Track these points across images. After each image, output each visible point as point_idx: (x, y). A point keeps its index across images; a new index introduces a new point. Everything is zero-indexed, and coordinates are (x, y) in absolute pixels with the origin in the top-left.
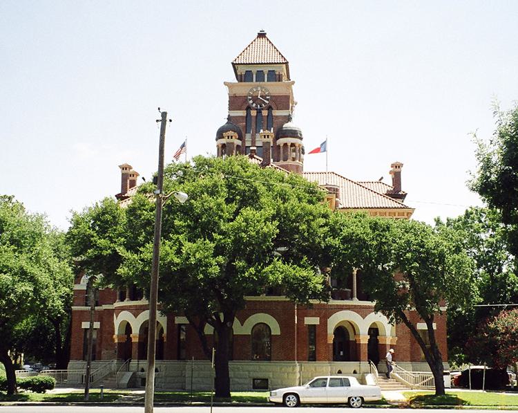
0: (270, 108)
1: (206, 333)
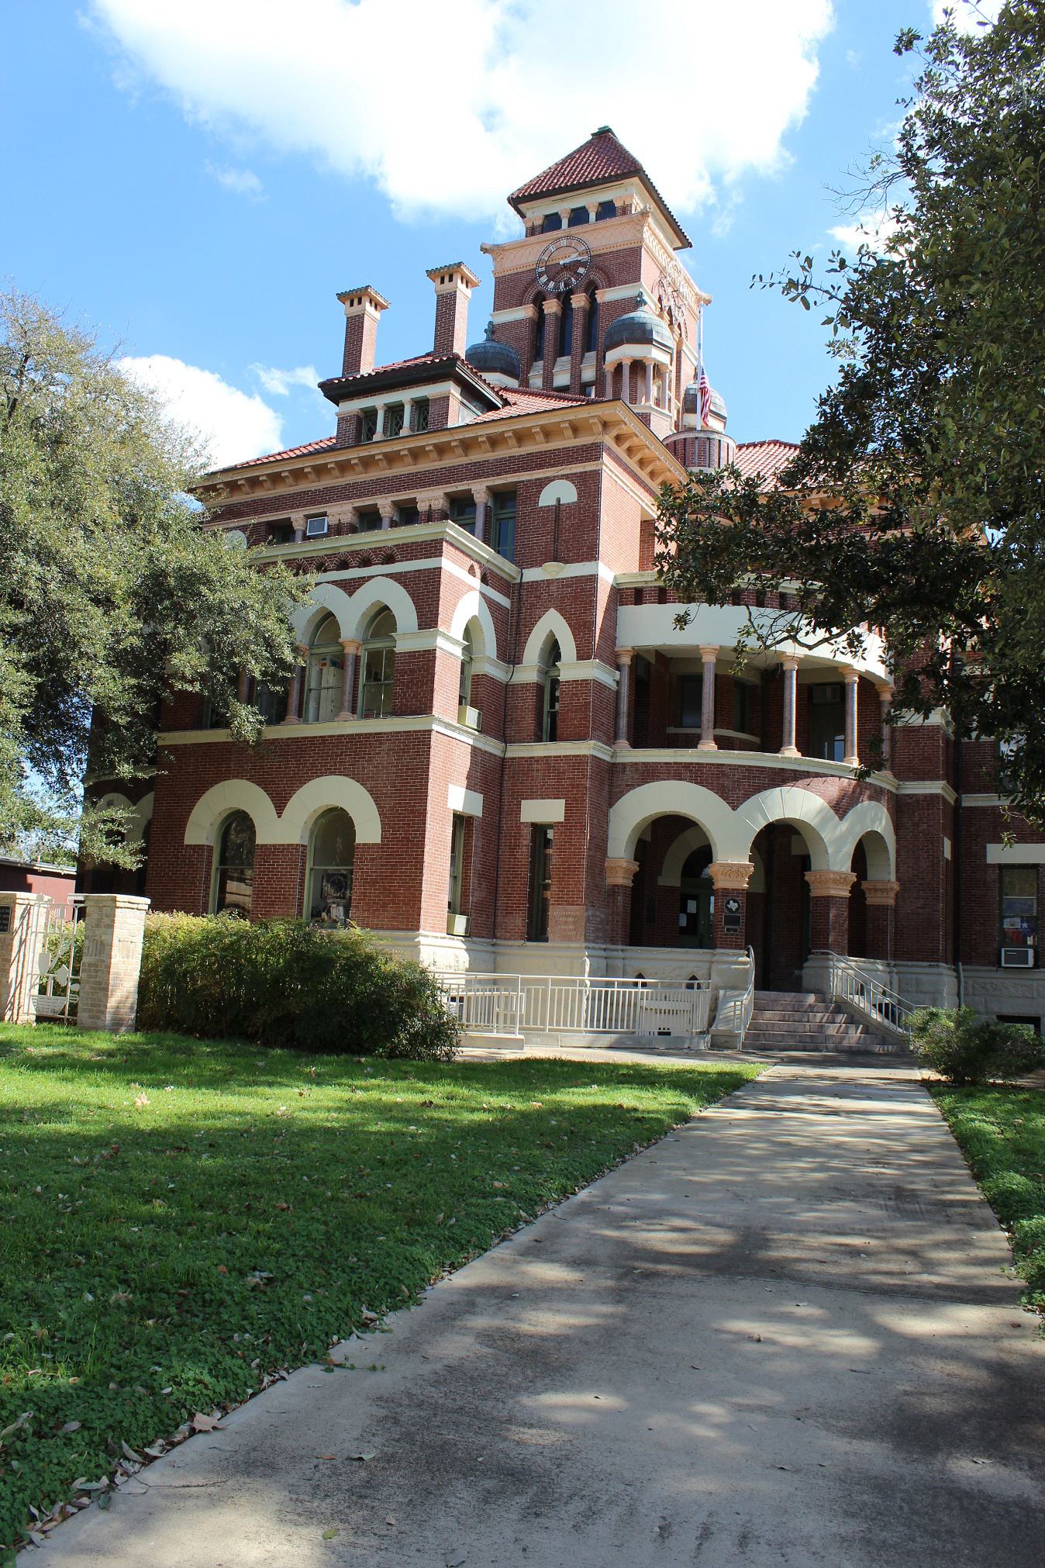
0: (591, 289)
1: (552, 610)
